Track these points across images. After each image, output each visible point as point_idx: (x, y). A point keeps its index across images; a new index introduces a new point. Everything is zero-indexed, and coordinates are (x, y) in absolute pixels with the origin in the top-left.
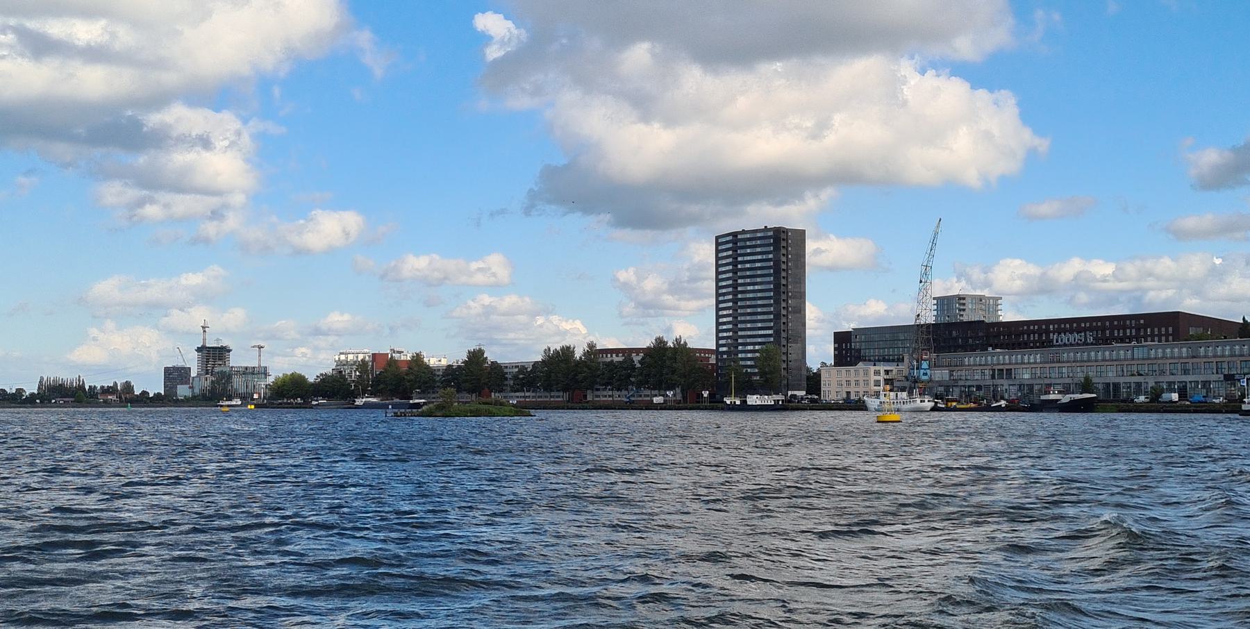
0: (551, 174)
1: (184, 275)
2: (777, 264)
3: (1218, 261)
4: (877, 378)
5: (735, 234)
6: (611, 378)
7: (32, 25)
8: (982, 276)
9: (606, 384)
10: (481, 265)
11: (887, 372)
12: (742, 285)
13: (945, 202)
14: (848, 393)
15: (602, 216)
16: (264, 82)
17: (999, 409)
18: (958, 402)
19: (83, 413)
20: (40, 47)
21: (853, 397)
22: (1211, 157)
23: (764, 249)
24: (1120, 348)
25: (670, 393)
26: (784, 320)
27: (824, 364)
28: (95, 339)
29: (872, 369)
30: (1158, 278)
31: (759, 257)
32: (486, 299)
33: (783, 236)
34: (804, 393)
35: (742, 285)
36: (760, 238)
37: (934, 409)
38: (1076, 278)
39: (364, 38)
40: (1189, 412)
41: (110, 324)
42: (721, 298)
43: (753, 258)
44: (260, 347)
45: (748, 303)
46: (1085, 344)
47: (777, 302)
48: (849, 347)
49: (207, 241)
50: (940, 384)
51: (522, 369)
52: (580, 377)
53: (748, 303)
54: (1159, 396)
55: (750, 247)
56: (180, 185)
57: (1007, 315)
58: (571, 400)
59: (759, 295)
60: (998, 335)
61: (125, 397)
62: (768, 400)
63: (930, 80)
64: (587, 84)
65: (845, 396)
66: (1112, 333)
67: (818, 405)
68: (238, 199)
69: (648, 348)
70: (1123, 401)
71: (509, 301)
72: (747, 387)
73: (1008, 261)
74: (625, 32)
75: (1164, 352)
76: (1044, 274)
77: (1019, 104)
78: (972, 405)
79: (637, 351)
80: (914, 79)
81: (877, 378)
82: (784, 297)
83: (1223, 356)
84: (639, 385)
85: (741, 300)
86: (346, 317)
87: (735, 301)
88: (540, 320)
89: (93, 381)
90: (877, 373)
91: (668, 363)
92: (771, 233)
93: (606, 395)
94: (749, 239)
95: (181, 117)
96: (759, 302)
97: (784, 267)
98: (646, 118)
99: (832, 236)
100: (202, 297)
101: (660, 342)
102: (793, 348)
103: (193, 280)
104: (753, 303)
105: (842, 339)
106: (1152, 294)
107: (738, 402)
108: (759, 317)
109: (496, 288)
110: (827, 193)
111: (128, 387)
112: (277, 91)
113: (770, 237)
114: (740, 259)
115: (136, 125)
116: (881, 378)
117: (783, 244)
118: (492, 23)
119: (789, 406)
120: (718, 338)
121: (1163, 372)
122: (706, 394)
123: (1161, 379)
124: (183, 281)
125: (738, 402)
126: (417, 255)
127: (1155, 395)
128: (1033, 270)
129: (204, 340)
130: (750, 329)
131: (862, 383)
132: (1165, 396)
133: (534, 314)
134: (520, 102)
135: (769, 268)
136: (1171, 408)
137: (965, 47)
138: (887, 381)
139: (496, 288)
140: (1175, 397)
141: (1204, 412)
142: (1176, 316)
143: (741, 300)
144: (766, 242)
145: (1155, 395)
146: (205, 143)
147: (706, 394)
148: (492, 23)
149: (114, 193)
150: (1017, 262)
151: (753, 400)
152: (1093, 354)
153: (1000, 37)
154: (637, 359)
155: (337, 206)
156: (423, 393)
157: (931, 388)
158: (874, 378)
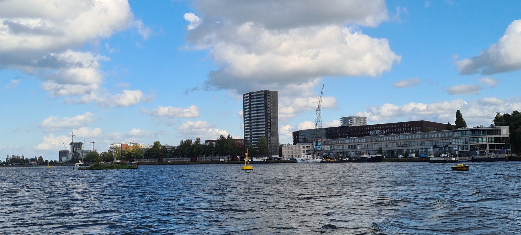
0: (212, 74)
1: (77, 116)
2: (266, 104)
3: (466, 103)
4: (304, 150)
5: (250, 94)
6: (204, 152)
7: (15, 21)
8: (377, 111)
9: (204, 154)
10: (188, 110)
11: (307, 147)
12: (253, 114)
13: (362, 81)
14: (292, 156)
15: (234, 90)
16: (103, 41)
17: (345, 161)
18: (331, 159)
19: (27, 169)
20: (17, 29)
21: (294, 157)
22: (466, 62)
25: (226, 157)
26: (269, 127)
27: (289, 144)
28: (45, 141)
29: (302, 146)
30: (443, 109)
32: (190, 123)
33: (268, 94)
35: (253, 114)
36: (259, 95)
37: (322, 162)
38: (413, 110)
39: (139, 23)
40: (418, 161)
41: (51, 135)
43: (257, 103)
44: (93, 142)
46: (382, 134)
47: (266, 120)
48: (298, 137)
49: (83, 103)
50: (326, 152)
51: (173, 148)
52: (193, 152)
54: (407, 155)
55: (255, 98)
56: (72, 81)
57: (368, 123)
58: (192, 161)
59: (259, 117)
60: (354, 132)
61: (40, 162)
62: (261, 159)
63: (356, 36)
64: (227, 39)
65: (291, 157)
66: (397, 130)
67: (281, 161)
68: (95, 86)
69: (218, 140)
70: (394, 157)
71: (198, 123)
73: (386, 104)
74: (241, 20)
75: (412, 137)
76: (400, 109)
77: (389, 44)
78: (336, 160)
79: (213, 141)
80: (350, 35)
81: (304, 150)
83: (418, 139)
84: (215, 154)
85: (253, 119)
86: (138, 131)
87: (250, 120)
88: (210, 130)
89: (28, 156)
90: (304, 148)
91: (225, 145)
92: (263, 93)
93: (203, 159)
95: (70, 55)
96: (260, 120)
98: (249, 52)
100: (84, 124)
101: (222, 137)
102: (273, 138)
103: (81, 117)
104: (257, 121)
105: (296, 135)
106: (441, 116)
108: (260, 126)
109: (193, 118)
110: (317, 80)
111: (41, 158)
112: (107, 46)
113: (263, 94)
115: (54, 59)
116: (305, 149)
117: (268, 97)
118: (190, 17)
119: (270, 161)
120: (245, 135)
121: (410, 145)
122: (238, 157)
123: (409, 148)
124: (77, 118)
125: (250, 160)
126: (164, 106)
127: (406, 155)
128: (396, 108)
129: (73, 140)
133: (208, 128)
134: (200, 47)
135: (263, 106)
136: (412, 160)
137: (370, 21)
138: (307, 151)
139: (193, 118)
140: (414, 155)
141: (409, 161)
142: (422, 122)
143: (253, 119)
144: (261, 96)
146: (80, 65)
147: (238, 157)
148: (190, 17)
149: (49, 85)
150: (390, 105)
151: (255, 159)
153: (383, 17)
154: (214, 144)
155: (133, 88)
156: (138, 159)
158: (302, 150)
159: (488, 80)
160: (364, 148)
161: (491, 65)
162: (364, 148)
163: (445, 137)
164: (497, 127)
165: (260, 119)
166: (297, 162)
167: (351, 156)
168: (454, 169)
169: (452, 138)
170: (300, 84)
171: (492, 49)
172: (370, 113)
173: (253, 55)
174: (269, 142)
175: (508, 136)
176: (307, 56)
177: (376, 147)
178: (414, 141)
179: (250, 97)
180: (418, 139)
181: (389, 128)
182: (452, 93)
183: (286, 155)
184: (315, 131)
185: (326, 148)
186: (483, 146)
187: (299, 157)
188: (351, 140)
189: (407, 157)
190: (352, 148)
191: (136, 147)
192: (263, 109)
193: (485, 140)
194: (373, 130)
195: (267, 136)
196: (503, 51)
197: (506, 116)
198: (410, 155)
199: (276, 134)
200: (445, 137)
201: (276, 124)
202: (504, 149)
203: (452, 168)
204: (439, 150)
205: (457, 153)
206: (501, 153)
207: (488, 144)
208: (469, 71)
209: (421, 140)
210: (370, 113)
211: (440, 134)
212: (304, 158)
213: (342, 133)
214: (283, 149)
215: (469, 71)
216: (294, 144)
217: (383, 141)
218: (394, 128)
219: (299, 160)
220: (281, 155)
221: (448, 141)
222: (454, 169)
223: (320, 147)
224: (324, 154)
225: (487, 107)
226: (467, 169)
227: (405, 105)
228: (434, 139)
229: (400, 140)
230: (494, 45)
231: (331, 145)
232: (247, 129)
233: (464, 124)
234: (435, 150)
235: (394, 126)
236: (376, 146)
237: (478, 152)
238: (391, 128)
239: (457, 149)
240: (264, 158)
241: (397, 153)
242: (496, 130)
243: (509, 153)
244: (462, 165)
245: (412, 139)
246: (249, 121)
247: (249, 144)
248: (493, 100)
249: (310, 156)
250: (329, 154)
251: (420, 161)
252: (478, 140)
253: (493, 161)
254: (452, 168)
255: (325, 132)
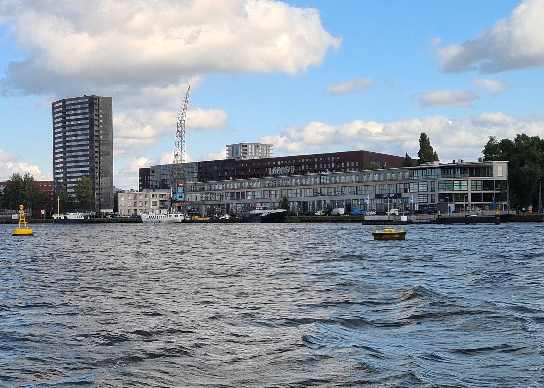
0: (15, 67)
2: (91, 120)
3: (450, 122)
4: (154, 200)
5: (64, 101)
13: (272, 82)
14: (136, 210)
17: (224, 221)
18: (200, 215)
22: (454, 50)
23: (83, 111)
24: (311, 177)
26: (96, 160)
27: (132, 190)
29: (151, 193)
31: (80, 117)
33: (95, 102)
34: (112, 211)
36: (80, 104)
38: (359, 133)
40: (348, 222)
42: (56, 146)
43: (78, 117)
45: (73, 149)
47: (92, 148)
50: (192, 203)
53: (73, 149)
54: (331, 210)
57: (275, 155)
59: (80, 143)
60: (243, 169)
62: (80, 216)
65: (133, 212)
67: (115, 220)
69: (9, 181)
72: (69, 207)
73: (370, 122)
75: (340, 179)
76: (337, 132)
77: (321, 18)
78: (208, 218)
81: (154, 200)
82: (96, 144)
83: (351, 182)
85: (69, 146)
87: (64, 148)
90: (154, 196)
92: (87, 100)
94: (73, 104)
96: (80, 148)
97: (96, 123)
98: (78, 29)
99: (199, 109)
101: (17, 177)
102: (104, 180)
107: (62, 218)
108: (80, 159)
113: (86, 103)
114: (67, 118)
116: (157, 199)
117: (96, 107)
120: (55, 174)
122: (43, 212)
123: (334, 198)
125: (62, 218)
127: (329, 211)
128: (329, 129)
130: (74, 167)
131: (144, 203)
132: (335, 211)
133: (6, 161)
135: (86, 124)
136: (338, 219)
138: (162, 202)
140: (342, 211)
142: (361, 153)
143: (69, 146)
144: (84, 106)
145: (329, 211)
147: (43, 212)
150: (319, 124)
151: (71, 216)
152: (294, 181)
157: (185, 207)
158: (152, 200)
159: (491, 83)
160: (258, 198)
161: (495, 57)
162: (258, 198)
163: (397, 180)
164: (488, 163)
165: (81, 145)
166: (141, 222)
167: (235, 211)
168: (379, 237)
169: (407, 182)
170: (165, 87)
171: (500, 28)
172: (285, 138)
173: (86, 34)
174: (97, 186)
175: (505, 178)
176: (179, 38)
177: (278, 196)
178: (339, 187)
179: (64, 107)
180: (351, 182)
181: (305, 164)
182: (426, 103)
183: (125, 210)
184: (175, 167)
185: (194, 197)
186: (464, 196)
187: (147, 212)
188: (236, 184)
189: (330, 214)
190: (238, 198)
191: (444, 174)
192: (86, 129)
193: (465, 186)
194: (277, 166)
195: (92, 177)
196: (518, 32)
197: (505, 143)
198: (334, 210)
199: (109, 173)
200: (397, 180)
201: (109, 154)
202: (496, 201)
203: (375, 235)
204: (384, 201)
205: (417, 208)
206: (491, 208)
207: (470, 193)
208: (458, 66)
209: (355, 185)
210: (285, 138)
211: (388, 175)
212: (154, 215)
213: (223, 172)
214: (121, 198)
215: (458, 66)
216: (141, 190)
217: (292, 186)
218: (313, 164)
219: (145, 217)
220: (116, 209)
221: (402, 186)
222: (379, 237)
223: (181, 196)
224: (189, 208)
225: (486, 129)
226: (401, 237)
227: (346, 125)
228: (378, 183)
229: (320, 184)
230: (503, 21)
231: (202, 191)
232: (58, 163)
233: (434, 157)
234: (379, 202)
235: (313, 160)
236: (278, 195)
237: (452, 206)
238: (309, 164)
239: (415, 201)
240: (86, 214)
241: (313, 208)
242: (484, 168)
243: (505, 209)
244: (394, 231)
245: (340, 182)
246: (61, 150)
247: (61, 189)
248: (498, 117)
249: (165, 211)
250: (198, 209)
251: (352, 221)
252: (453, 184)
253: (445, 223)
254: (375, 235)
255: (196, 169)
